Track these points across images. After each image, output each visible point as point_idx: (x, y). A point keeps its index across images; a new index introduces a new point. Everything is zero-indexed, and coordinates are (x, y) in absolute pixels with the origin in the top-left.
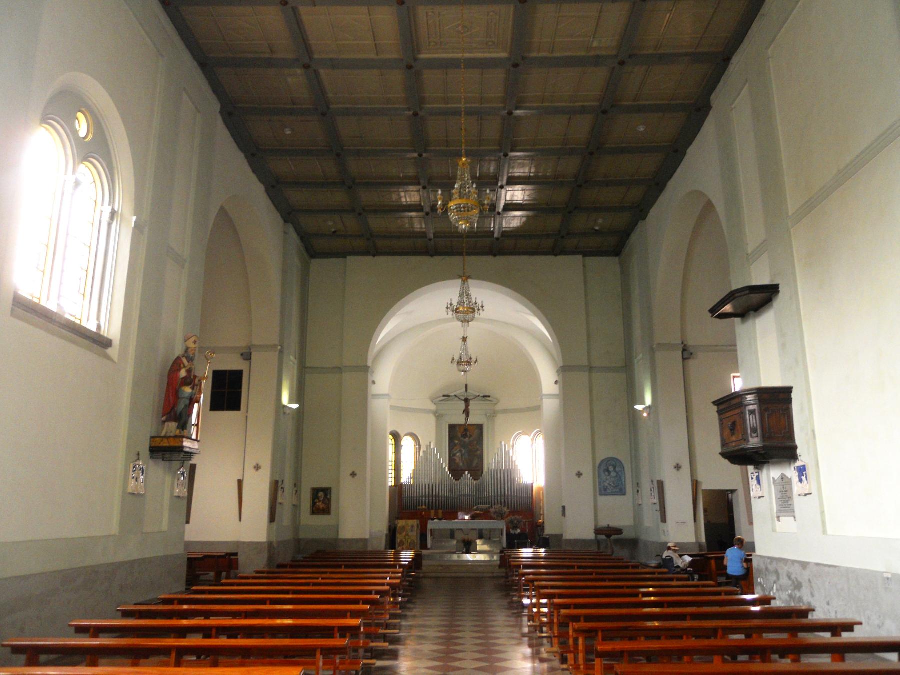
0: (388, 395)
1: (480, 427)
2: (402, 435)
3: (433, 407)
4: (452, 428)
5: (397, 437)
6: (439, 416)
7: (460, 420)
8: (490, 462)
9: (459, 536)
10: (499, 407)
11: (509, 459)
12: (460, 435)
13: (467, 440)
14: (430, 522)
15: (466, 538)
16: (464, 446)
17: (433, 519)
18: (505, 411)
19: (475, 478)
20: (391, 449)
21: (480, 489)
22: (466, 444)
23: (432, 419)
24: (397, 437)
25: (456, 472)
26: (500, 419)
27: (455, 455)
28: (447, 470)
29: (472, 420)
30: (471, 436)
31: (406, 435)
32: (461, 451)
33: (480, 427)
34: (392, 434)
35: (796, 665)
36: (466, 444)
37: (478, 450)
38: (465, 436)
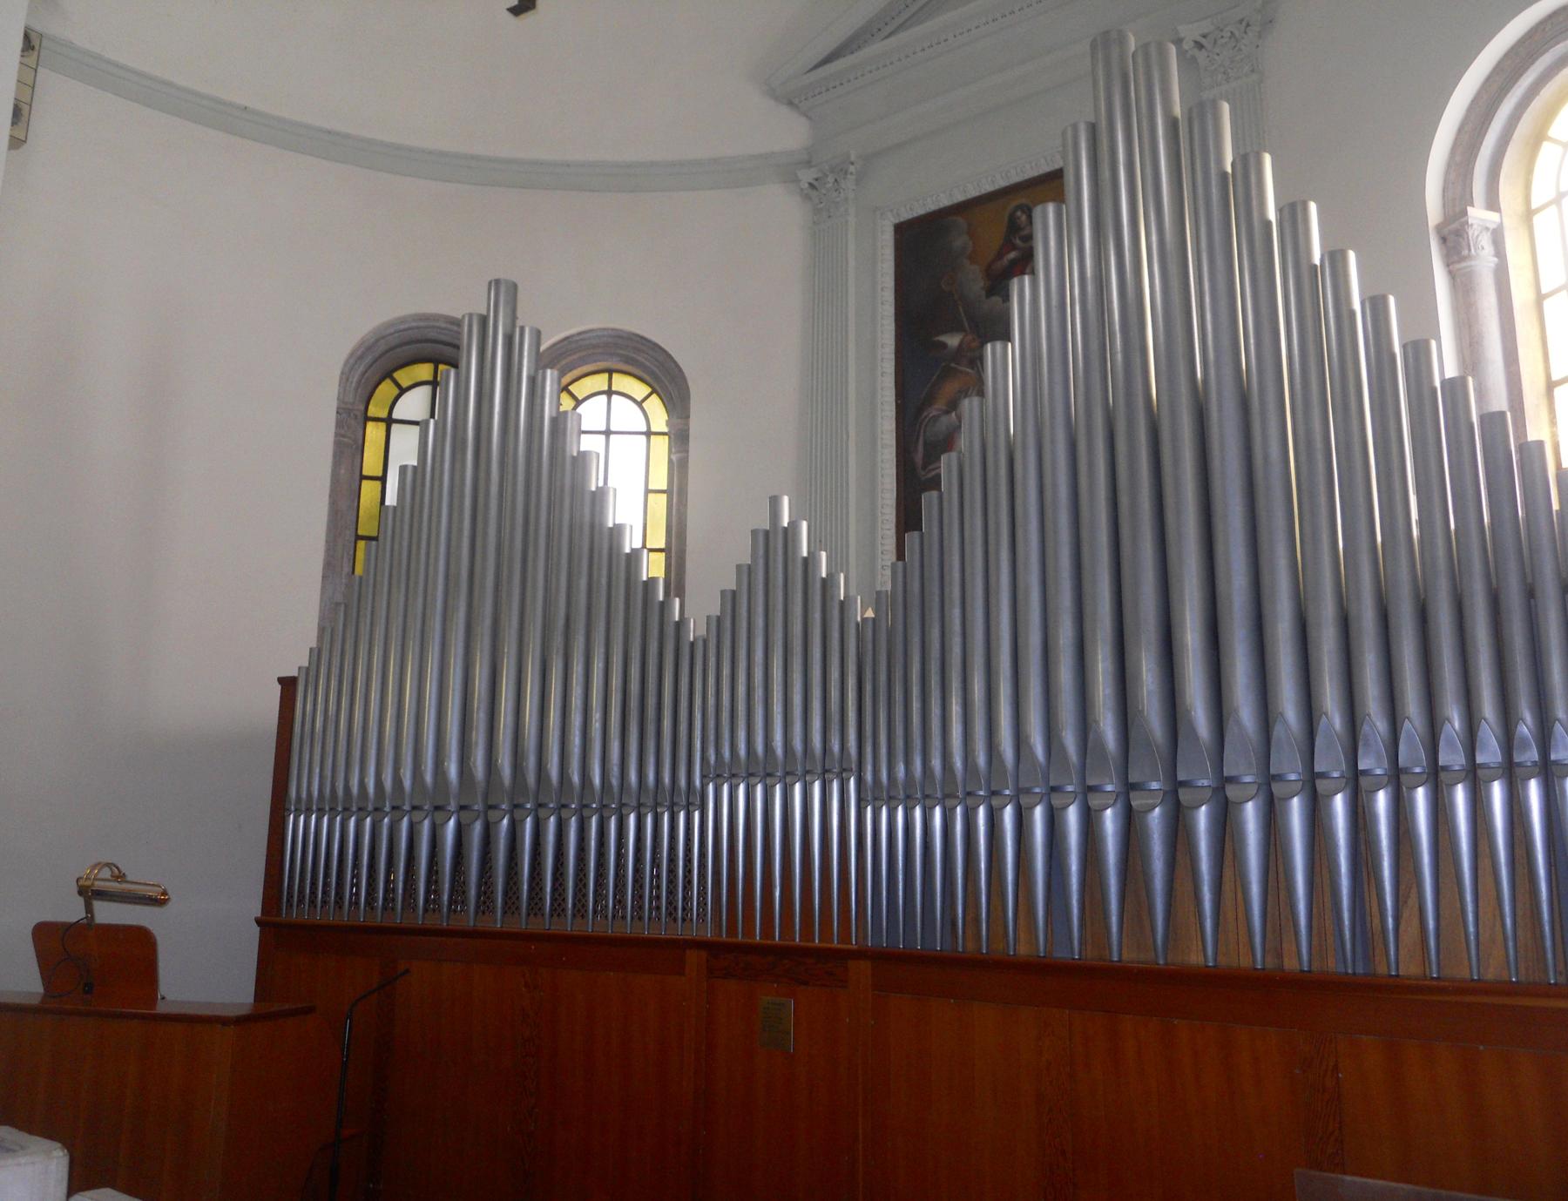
3: (787, 133)
6: (821, 181)
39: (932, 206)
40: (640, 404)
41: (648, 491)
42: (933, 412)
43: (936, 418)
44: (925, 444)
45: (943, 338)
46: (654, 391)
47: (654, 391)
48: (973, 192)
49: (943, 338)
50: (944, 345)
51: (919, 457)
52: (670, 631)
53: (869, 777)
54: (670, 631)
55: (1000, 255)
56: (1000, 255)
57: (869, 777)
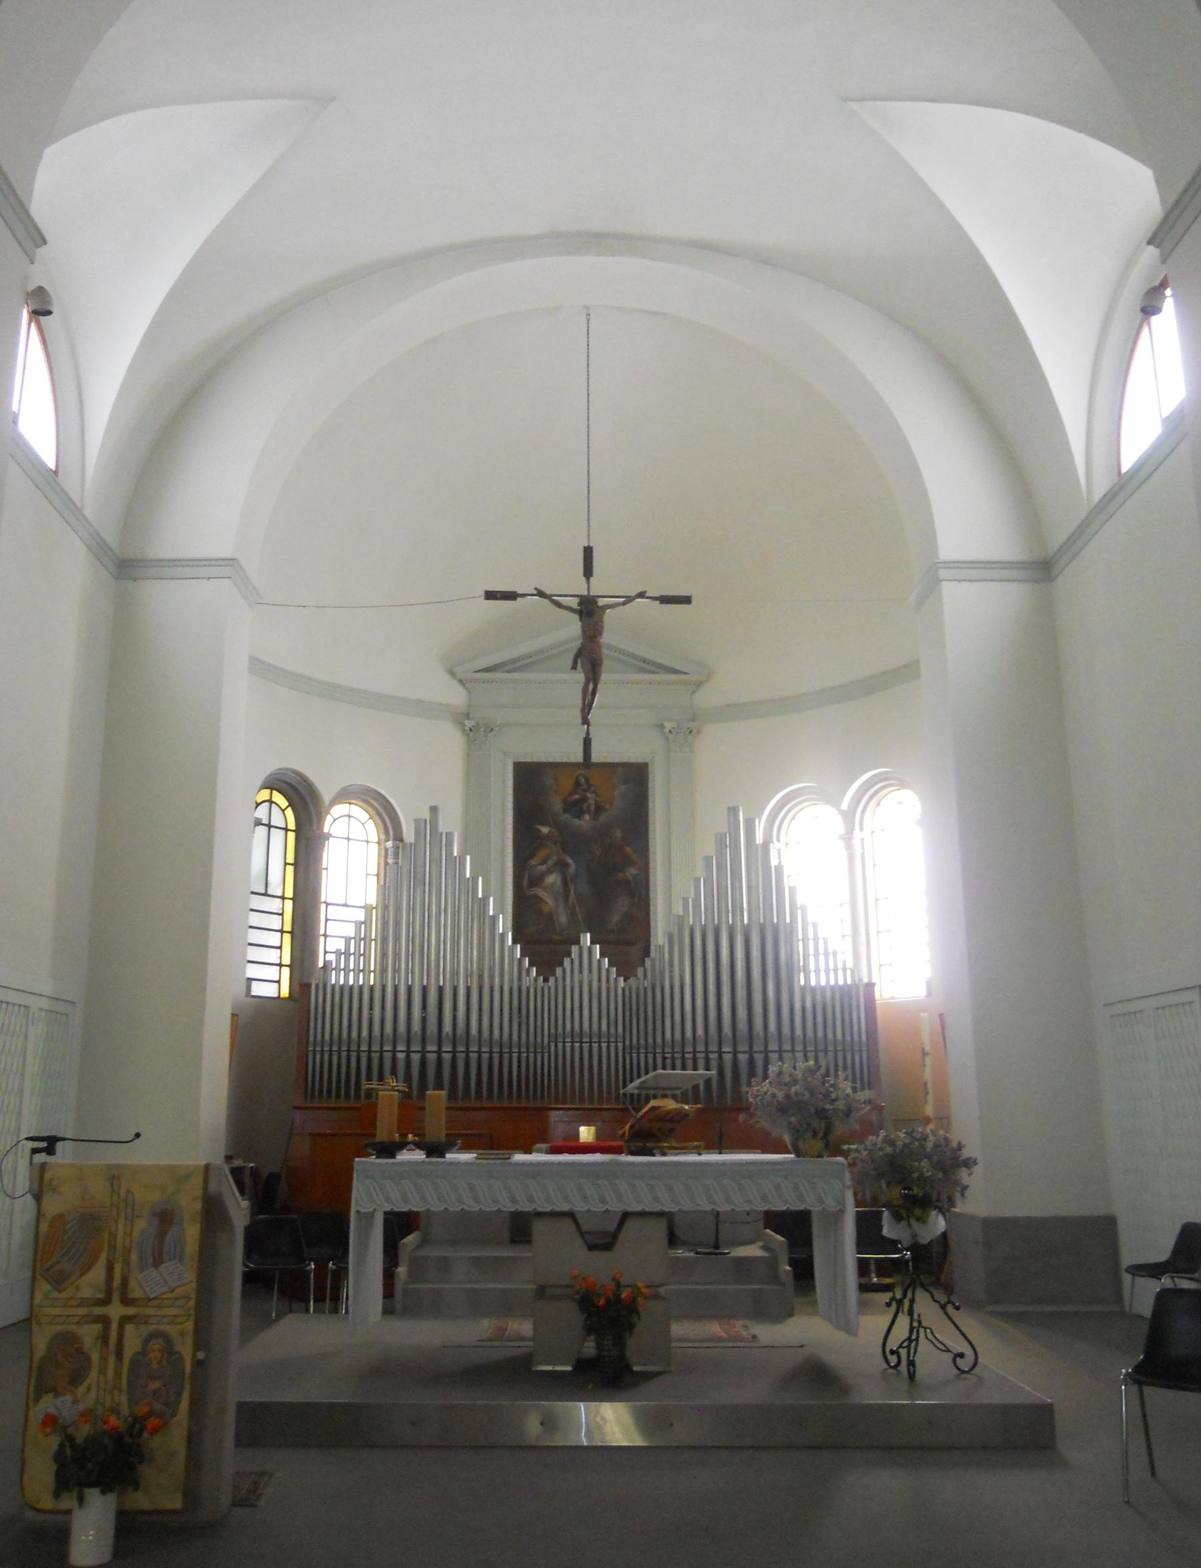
0: (231, 561)
1: (636, 776)
2: (326, 795)
3: (456, 696)
4: (530, 779)
5: (304, 800)
6: (476, 730)
7: (563, 747)
8: (676, 892)
9: (562, 1257)
10: (708, 698)
11: (767, 878)
12: (557, 804)
13: (585, 822)
14: (367, 1165)
15: (599, 1269)
16: (572, 843)
17: (388, 1150)
18: (734, 712)
19: (625, 968)
20: (271, 856)
21: (641, 1010)
22: (581, 840)
23: (451, 741)
24: (304, 800)
25: (541, 940)
26: (715, 746)
27: (537, 881)
28: (504, 925)
29: (610, 748)
30: (599, 809)
31: (345, 795)
32: (561, 866)
33: (636, 776)
34: (273, 784)
35: (599, 1257)
36: (581, 840)
37: (628, 861)
38: (575, 807)
39: (543, 759)
40: (283, 811)
41: (286, 864)
42: (533, 862)
43: (536, 866)
44: (529, 877)
45: (540, 827)
46: (279, 997)
47: (279, 997)
48: (558, 760)
49: (540, 827)
50: (540, 831)
51: (525, 882)
52: (329, 991)
53: (627, 1042)
54: (329, 991)
55: (571, 794)
56: (571, 794)
57: (627, 1042)
